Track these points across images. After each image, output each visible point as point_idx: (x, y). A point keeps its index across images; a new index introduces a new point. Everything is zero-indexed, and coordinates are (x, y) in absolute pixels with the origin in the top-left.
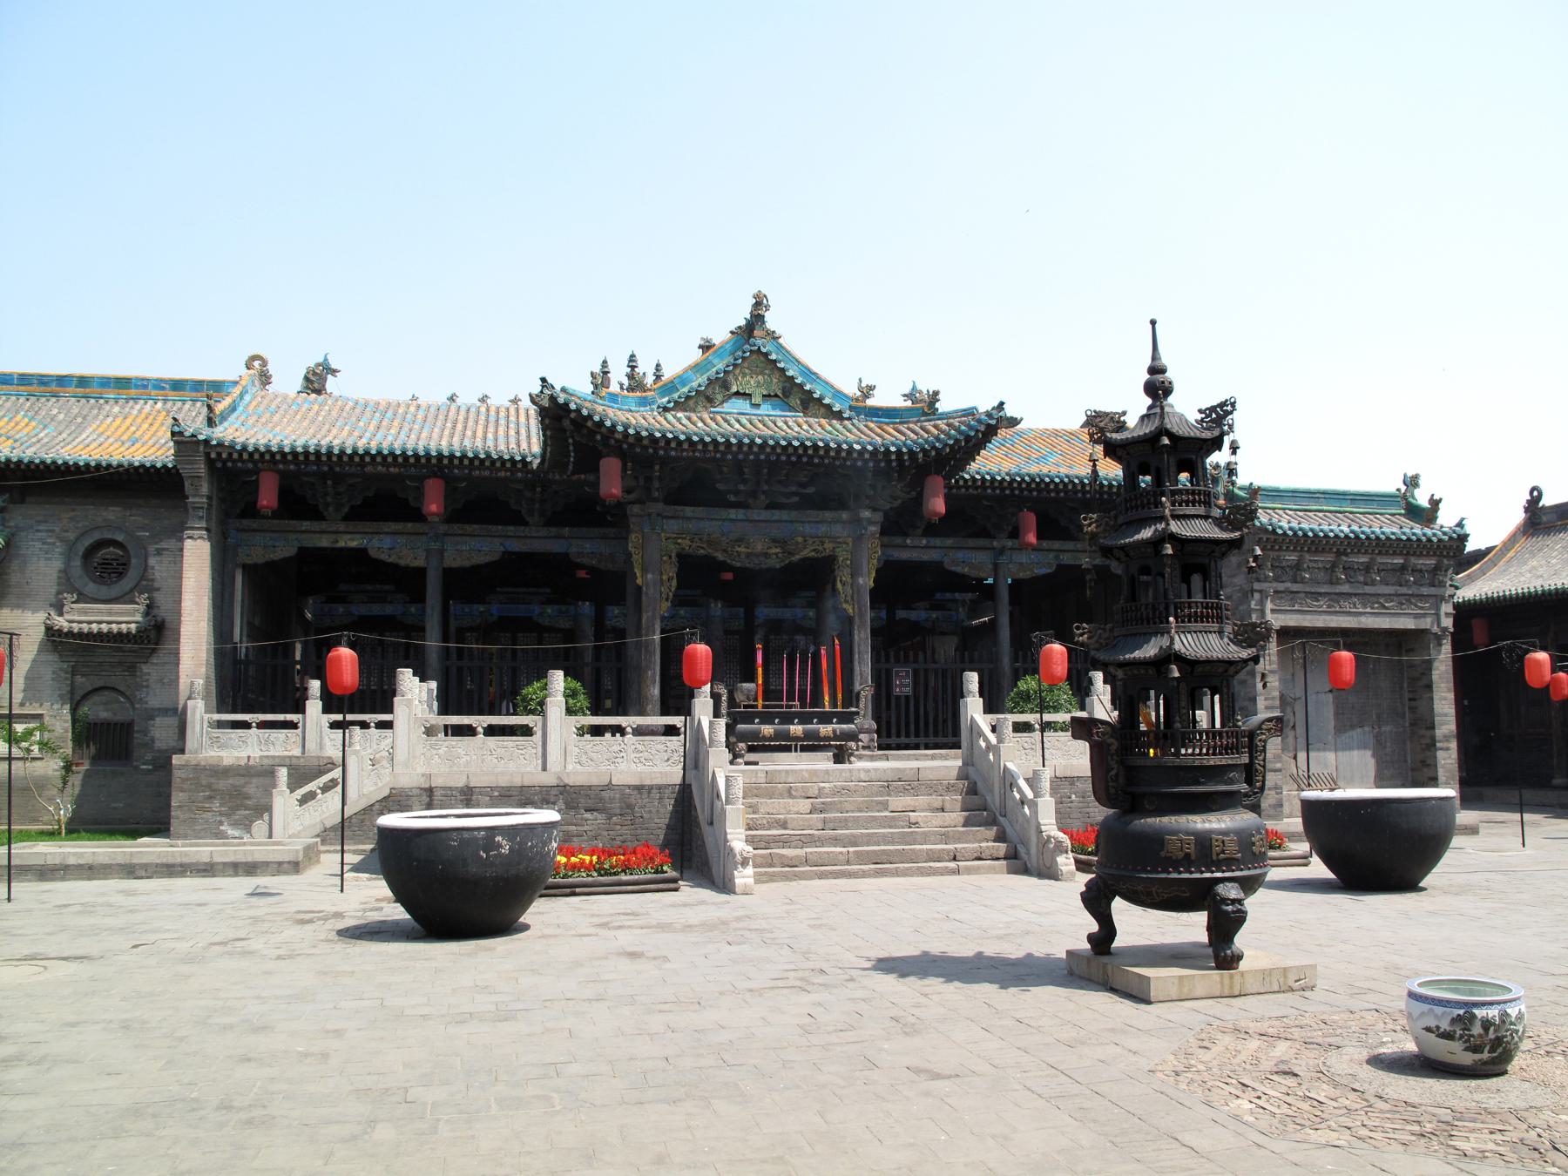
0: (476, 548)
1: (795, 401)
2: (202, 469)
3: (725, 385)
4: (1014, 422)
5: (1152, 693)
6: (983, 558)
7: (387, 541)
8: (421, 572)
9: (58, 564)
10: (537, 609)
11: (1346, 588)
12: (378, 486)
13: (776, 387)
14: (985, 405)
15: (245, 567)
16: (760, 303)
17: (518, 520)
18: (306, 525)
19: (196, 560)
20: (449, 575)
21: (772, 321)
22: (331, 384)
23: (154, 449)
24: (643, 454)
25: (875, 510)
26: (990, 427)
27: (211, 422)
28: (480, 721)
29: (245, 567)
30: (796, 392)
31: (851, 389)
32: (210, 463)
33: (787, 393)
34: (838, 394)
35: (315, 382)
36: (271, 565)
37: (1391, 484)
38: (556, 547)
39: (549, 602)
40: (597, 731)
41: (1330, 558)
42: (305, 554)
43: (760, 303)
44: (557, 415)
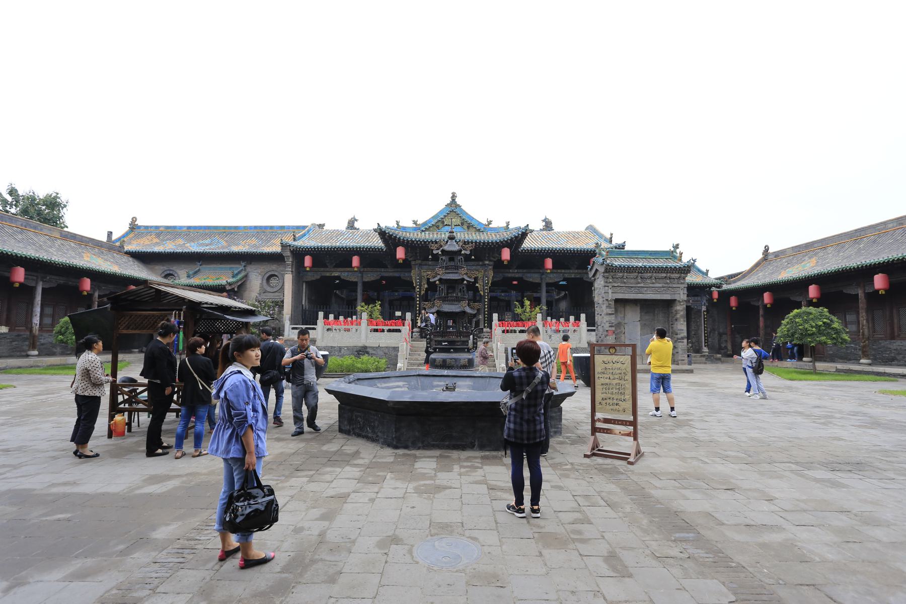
0: (371, 276)
1: (465, 227)
2: (289, 254)
3: (443, 222)
4: (532, 231)
5: (321, 314)
6: (536, 275)
7: (346, 274)
8: (355, 284)
9: (260, 282)
10: (499, 294)
11: (642, 285)
12: (337, 257)
13: (459, 223)
14: (523, 226)
15: (306, 282)
16: (454, 196)
17: (385, 267)
18: (322, 269)
19: (288, 279)
20: (365, 284)
21: (458, 201)
22: (356, 225)
23: (277, 249)
24: (413, 247)
25: (490, 261)
26: (524, 234)
27: (295, 240)
28: (386, 328)
29: (306, 282)
30: (468, 224)
31: (485, 222)
32: (292, 252)
33: (462, 224)
34: (480, 223)
35: (548, 225)
36: (312, 281)
37: (668, 247)
38: (396, 275)
39: (502, 292)
40: (376, 330)
41: (636, 274)
42: (322, 277)
43: (454, 196)
44: (382, 233)
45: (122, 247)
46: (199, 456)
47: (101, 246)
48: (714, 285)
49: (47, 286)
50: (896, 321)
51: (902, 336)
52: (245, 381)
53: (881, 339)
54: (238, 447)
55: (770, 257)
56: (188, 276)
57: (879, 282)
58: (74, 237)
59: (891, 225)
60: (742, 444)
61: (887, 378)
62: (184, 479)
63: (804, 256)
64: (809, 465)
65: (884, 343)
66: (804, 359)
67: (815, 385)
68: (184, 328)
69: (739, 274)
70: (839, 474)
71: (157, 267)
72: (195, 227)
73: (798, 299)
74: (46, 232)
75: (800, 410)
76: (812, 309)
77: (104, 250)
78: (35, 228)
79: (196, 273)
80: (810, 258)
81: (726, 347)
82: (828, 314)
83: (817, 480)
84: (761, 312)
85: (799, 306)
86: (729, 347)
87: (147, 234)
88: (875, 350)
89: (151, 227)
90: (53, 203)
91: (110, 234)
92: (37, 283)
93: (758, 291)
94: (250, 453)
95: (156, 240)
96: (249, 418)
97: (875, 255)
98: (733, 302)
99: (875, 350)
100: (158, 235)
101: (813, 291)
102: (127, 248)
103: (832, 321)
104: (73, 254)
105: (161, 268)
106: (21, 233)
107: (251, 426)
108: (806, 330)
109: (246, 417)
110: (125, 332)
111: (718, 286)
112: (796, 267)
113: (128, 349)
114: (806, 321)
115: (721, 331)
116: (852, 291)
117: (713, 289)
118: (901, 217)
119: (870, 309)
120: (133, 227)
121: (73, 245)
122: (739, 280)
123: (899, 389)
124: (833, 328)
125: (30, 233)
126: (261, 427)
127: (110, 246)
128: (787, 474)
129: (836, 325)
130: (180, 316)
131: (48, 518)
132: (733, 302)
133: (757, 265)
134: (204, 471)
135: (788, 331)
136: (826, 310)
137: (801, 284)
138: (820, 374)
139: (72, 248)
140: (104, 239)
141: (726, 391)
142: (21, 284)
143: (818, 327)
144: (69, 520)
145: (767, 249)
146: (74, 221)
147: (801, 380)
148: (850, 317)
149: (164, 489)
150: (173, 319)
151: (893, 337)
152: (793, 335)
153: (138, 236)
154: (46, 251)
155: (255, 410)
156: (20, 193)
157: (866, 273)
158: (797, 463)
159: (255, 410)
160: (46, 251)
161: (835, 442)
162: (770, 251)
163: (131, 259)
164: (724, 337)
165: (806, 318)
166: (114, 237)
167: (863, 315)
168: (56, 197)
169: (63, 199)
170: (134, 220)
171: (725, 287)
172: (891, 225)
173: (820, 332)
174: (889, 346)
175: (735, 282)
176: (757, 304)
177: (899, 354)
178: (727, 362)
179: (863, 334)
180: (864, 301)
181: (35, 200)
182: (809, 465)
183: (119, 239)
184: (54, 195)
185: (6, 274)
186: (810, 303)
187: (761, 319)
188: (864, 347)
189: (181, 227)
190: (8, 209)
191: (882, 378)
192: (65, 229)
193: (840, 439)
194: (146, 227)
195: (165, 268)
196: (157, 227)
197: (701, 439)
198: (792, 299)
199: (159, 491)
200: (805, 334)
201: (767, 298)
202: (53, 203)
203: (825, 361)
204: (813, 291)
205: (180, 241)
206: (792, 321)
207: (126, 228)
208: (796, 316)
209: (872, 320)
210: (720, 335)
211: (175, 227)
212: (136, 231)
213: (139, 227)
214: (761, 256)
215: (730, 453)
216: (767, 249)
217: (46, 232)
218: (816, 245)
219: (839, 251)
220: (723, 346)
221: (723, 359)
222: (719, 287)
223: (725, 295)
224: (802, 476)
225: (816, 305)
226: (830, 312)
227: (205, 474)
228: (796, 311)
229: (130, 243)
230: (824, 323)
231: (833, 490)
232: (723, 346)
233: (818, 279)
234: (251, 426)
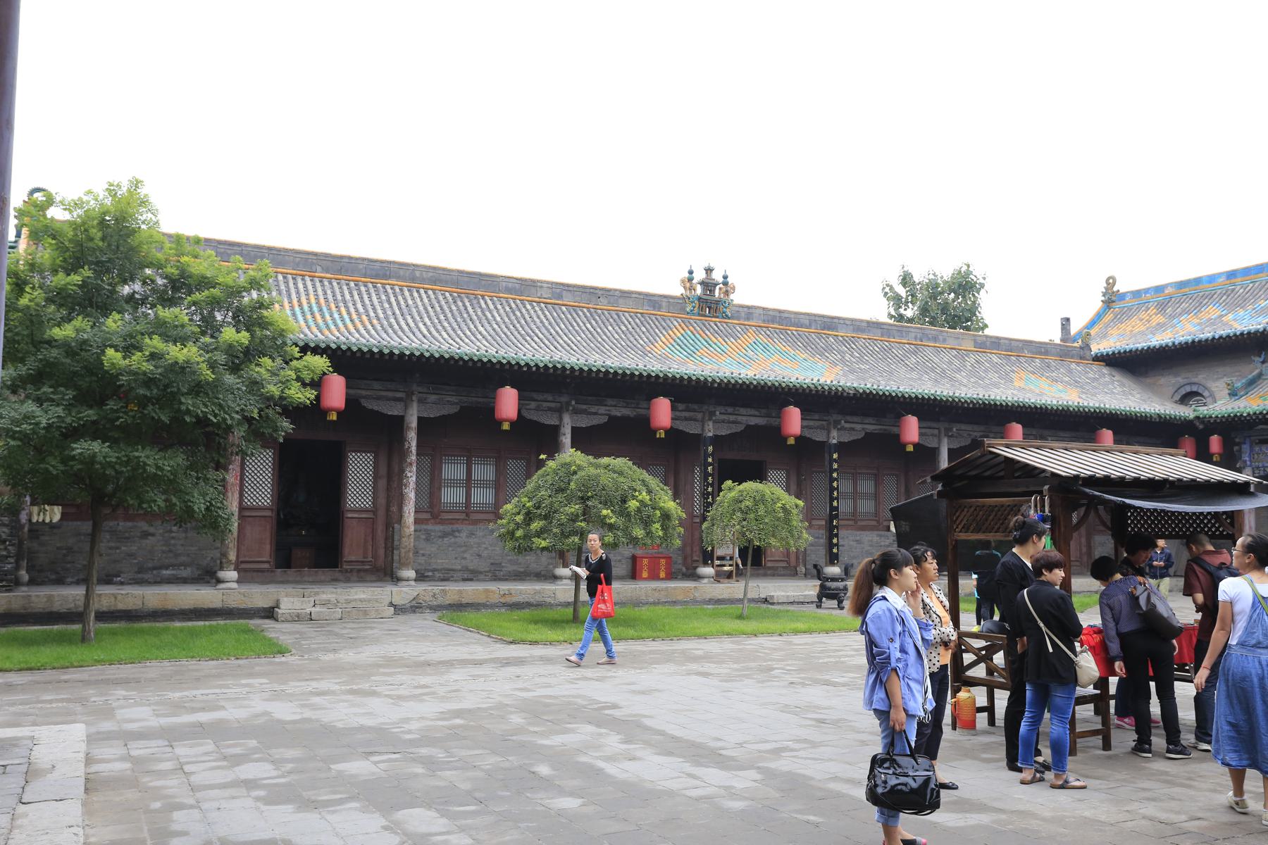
45: (1086, 347)
46: (1061, 787)
47: (1047, 353)
49: (955, 446)
52: (890, 610)
54: (883, 695)
56: (1233, 394)
58: (997, 344)
62: (1004, 817)
68: (1051, 529)
71: (1162, 380)
72: (1247, 271)
74: (951, 343)
77: (1051, 360)
78: (935, 339)
79: (1252, 383)
84: (412, 437)
87: (1138, 309)
89: (1147, 291)
90: (965, 285)
91: (1066, 322)
92: (940, 442)
94: (896, 707)
95: (1160, 319)
96: (893, 660)
100: (1162, 307)
102: (1098, 347)
104: (995, 377)
105: (1172, 381)
106: (915, 353)
107: (895, 670)
109: (889, 658)
110: (963, 536)
113: (969, 569)
120: (1111, 298)
121: (995, 359)
125: (928, 351)
126: (915, 675)
127: (1070, 350)
130: (1043, 506)
131: (799, 816)
134: (1047, 814)
139: (994, 365)
140: (1055, 336)
142: (916, 445)
144: (817, 825)
146: (1000, 315)
149: (961, 823)
150: (1032, 512)
153: (1120, 318)
154: (951, 379)
155: (903, 650)
156: (916, 279)
159: (903, 650)
160: (951, 379)
163: (1106, 370)
166: (1074, 329)
168: (968, 273)
169: (978, 273)
170: (1111, 282)
181: (937, 285)
183: (1079, 333)
184: (964, 268)
185: (895, 430)
189: (1212, 278)
190: (902, 311)
192: (987, 332)
194: (1136, 294)
195: (1181, 380)
196: (1159, 289)
199: (950, 824)
202: (965, 285)
205: (1212, 312)
207: (1096, 303)
211: (1198, 281)
212: (1117, 306)
213: (1122, 296)
217: (951, 343)
227: (1044, 819)
229: (1104, 336)
234: (895, 670)
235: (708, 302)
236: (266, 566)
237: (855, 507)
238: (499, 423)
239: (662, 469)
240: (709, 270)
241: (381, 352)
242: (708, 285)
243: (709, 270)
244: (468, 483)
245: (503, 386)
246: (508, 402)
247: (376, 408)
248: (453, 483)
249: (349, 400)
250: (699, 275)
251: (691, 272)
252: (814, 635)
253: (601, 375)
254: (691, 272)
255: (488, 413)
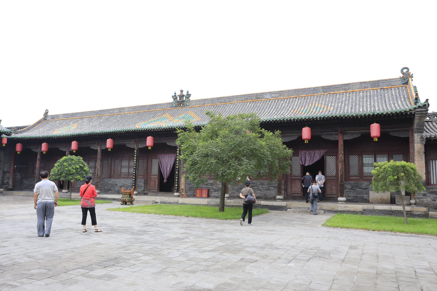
48: (5, 133)
50: (113, 167)
51: (115, 176)
53: (105, 178)
55: (48, 118)
57: (109, 143)
59: (116, 112)
60: (40, 261)
61: (108, 201)
63: (70, 121)
64: (90, 267)
65: (106, 180)
66: (64, 191)
67: (73, 208)
69: (24, 127)
70: (109, 269)
73: (64, 149)
75: (70, 227)
76: (74, 157)
80: (74, 123)
81: (8, 183)
82: (82, 161)
83: (100, 278)
84: (38, 157)
85: (64, 154)
86: (11, 183)
88: (101, 184)
93: (38, 141)
97: (108, 127)
98: (19, 147)
99: (101, 184)
101: (74, 145)
103: (84, 166)
108: (70, 171)
111: (8, 134)
112: (65, 128)
114: (70, 165)
115: (6, 170)
116: (94, 147)
117: (4, 136)
118: (121, 108)
119: (102, 160)
122: (24, 131)
123: (115, 207)
124: (84, 170)
128: (80, 278)
129: (86, 168)
132: (19, 147)
133: (39, 122)
135: (58, 171)
136: (81, 158)
137: (66, 140)
138: (372, 203)
141: (14, 218)
143: (76, 169)
145: (46, 113)
147: (64, 205)
148: (92, 164)
151: (110, 177)
152: (61, 174)
157: (101, 137)
158: (83, 268)
161: (98, 246)
162: (49, 114)
164: (7, 175)
165: (70, 162)
167: (99, 163)
171: (13, 136)
172: (116, 112)
173: (77, 173)
174: (108, 182)
175: (21, 132)
176: (36, 151)
177: (112, 187)
178: (7, 195)
179: (97, 175)
180: (100, 154)
182: (90, 267)
186: (71, 153)
187: (38, 162)
188: (97, 182)
191: (106, 201)
193: (100, 244)
197: (4, 264)
198: (60, 149)
200: (69, 173)
201: (44, 147)
203: (112, 193)
204: (74, 145)
206: (61, 165)
208: (64, 161)
209: (102, 166)
210: (4, 173)
214: (42, 116)
215: (33, 271)
216: (46, 113)
218: (77, 115)
219: (90, 122)
220: (6, 181)
221: (4, 192)
222: (8, 135)
223: (13, 142)
224: (89, 277)
225: (76, 154)
226: (84, 160)
228: (64, 158)
230: (80, 167)
231: (110, 282)
232: (6, 181)
233: (79, 138)
235: (181, 101)
236: (156, 191)
237: (129, 170)
238: (372, 138)
239: (401, 156)
240: (182, 91)
241: (172, 128)
242: (182, 96)
243: (182, 91)
244: (129, 167)
245: (373, 123)
246: (375, 130)
247: (328, 138)
248: (125, 167)
249: (381, 133)
250: (178, 93)
251: (175, 94)
252: (350, 230)
253: (318, 119)
254: (175, 94)
255: (367, 136)
